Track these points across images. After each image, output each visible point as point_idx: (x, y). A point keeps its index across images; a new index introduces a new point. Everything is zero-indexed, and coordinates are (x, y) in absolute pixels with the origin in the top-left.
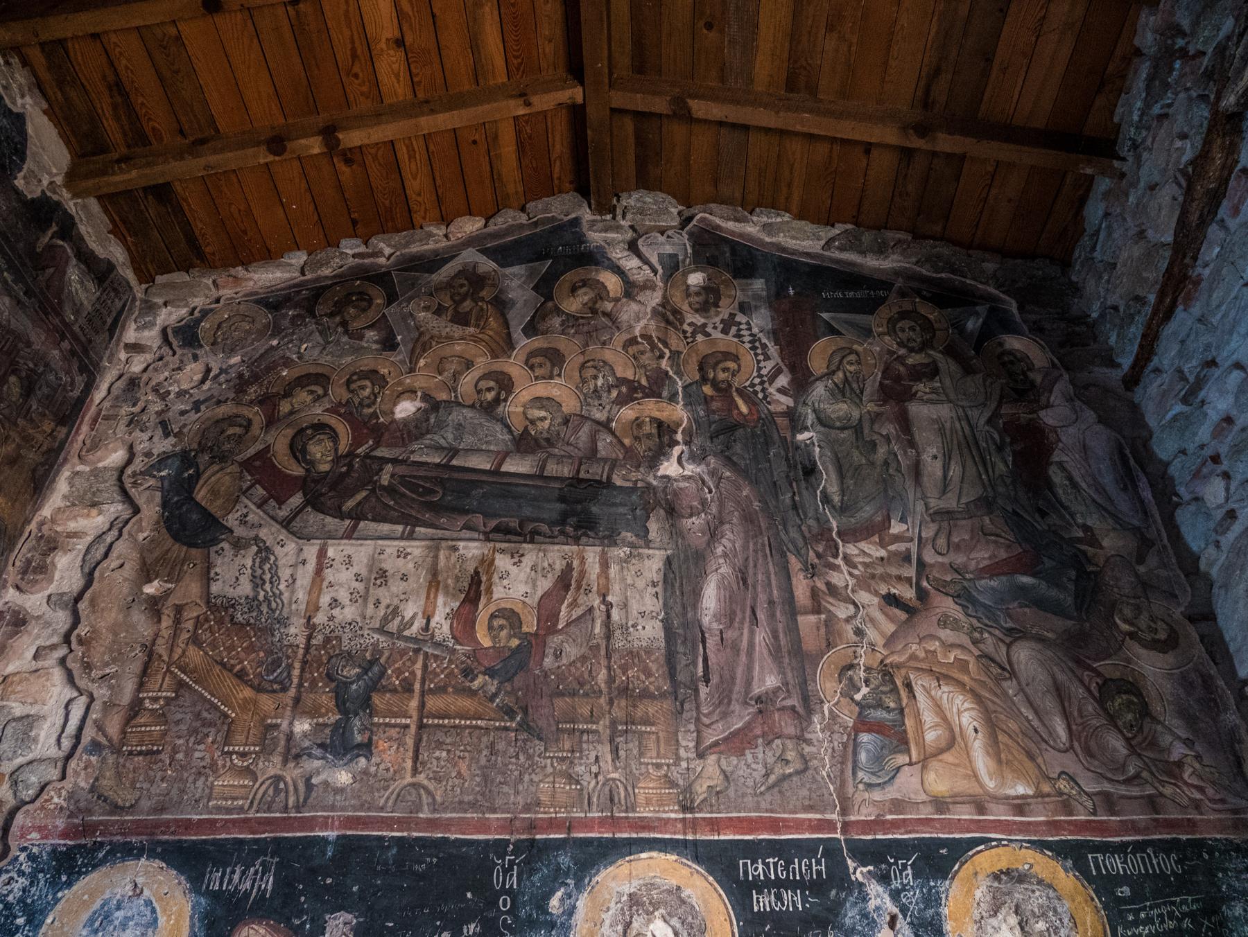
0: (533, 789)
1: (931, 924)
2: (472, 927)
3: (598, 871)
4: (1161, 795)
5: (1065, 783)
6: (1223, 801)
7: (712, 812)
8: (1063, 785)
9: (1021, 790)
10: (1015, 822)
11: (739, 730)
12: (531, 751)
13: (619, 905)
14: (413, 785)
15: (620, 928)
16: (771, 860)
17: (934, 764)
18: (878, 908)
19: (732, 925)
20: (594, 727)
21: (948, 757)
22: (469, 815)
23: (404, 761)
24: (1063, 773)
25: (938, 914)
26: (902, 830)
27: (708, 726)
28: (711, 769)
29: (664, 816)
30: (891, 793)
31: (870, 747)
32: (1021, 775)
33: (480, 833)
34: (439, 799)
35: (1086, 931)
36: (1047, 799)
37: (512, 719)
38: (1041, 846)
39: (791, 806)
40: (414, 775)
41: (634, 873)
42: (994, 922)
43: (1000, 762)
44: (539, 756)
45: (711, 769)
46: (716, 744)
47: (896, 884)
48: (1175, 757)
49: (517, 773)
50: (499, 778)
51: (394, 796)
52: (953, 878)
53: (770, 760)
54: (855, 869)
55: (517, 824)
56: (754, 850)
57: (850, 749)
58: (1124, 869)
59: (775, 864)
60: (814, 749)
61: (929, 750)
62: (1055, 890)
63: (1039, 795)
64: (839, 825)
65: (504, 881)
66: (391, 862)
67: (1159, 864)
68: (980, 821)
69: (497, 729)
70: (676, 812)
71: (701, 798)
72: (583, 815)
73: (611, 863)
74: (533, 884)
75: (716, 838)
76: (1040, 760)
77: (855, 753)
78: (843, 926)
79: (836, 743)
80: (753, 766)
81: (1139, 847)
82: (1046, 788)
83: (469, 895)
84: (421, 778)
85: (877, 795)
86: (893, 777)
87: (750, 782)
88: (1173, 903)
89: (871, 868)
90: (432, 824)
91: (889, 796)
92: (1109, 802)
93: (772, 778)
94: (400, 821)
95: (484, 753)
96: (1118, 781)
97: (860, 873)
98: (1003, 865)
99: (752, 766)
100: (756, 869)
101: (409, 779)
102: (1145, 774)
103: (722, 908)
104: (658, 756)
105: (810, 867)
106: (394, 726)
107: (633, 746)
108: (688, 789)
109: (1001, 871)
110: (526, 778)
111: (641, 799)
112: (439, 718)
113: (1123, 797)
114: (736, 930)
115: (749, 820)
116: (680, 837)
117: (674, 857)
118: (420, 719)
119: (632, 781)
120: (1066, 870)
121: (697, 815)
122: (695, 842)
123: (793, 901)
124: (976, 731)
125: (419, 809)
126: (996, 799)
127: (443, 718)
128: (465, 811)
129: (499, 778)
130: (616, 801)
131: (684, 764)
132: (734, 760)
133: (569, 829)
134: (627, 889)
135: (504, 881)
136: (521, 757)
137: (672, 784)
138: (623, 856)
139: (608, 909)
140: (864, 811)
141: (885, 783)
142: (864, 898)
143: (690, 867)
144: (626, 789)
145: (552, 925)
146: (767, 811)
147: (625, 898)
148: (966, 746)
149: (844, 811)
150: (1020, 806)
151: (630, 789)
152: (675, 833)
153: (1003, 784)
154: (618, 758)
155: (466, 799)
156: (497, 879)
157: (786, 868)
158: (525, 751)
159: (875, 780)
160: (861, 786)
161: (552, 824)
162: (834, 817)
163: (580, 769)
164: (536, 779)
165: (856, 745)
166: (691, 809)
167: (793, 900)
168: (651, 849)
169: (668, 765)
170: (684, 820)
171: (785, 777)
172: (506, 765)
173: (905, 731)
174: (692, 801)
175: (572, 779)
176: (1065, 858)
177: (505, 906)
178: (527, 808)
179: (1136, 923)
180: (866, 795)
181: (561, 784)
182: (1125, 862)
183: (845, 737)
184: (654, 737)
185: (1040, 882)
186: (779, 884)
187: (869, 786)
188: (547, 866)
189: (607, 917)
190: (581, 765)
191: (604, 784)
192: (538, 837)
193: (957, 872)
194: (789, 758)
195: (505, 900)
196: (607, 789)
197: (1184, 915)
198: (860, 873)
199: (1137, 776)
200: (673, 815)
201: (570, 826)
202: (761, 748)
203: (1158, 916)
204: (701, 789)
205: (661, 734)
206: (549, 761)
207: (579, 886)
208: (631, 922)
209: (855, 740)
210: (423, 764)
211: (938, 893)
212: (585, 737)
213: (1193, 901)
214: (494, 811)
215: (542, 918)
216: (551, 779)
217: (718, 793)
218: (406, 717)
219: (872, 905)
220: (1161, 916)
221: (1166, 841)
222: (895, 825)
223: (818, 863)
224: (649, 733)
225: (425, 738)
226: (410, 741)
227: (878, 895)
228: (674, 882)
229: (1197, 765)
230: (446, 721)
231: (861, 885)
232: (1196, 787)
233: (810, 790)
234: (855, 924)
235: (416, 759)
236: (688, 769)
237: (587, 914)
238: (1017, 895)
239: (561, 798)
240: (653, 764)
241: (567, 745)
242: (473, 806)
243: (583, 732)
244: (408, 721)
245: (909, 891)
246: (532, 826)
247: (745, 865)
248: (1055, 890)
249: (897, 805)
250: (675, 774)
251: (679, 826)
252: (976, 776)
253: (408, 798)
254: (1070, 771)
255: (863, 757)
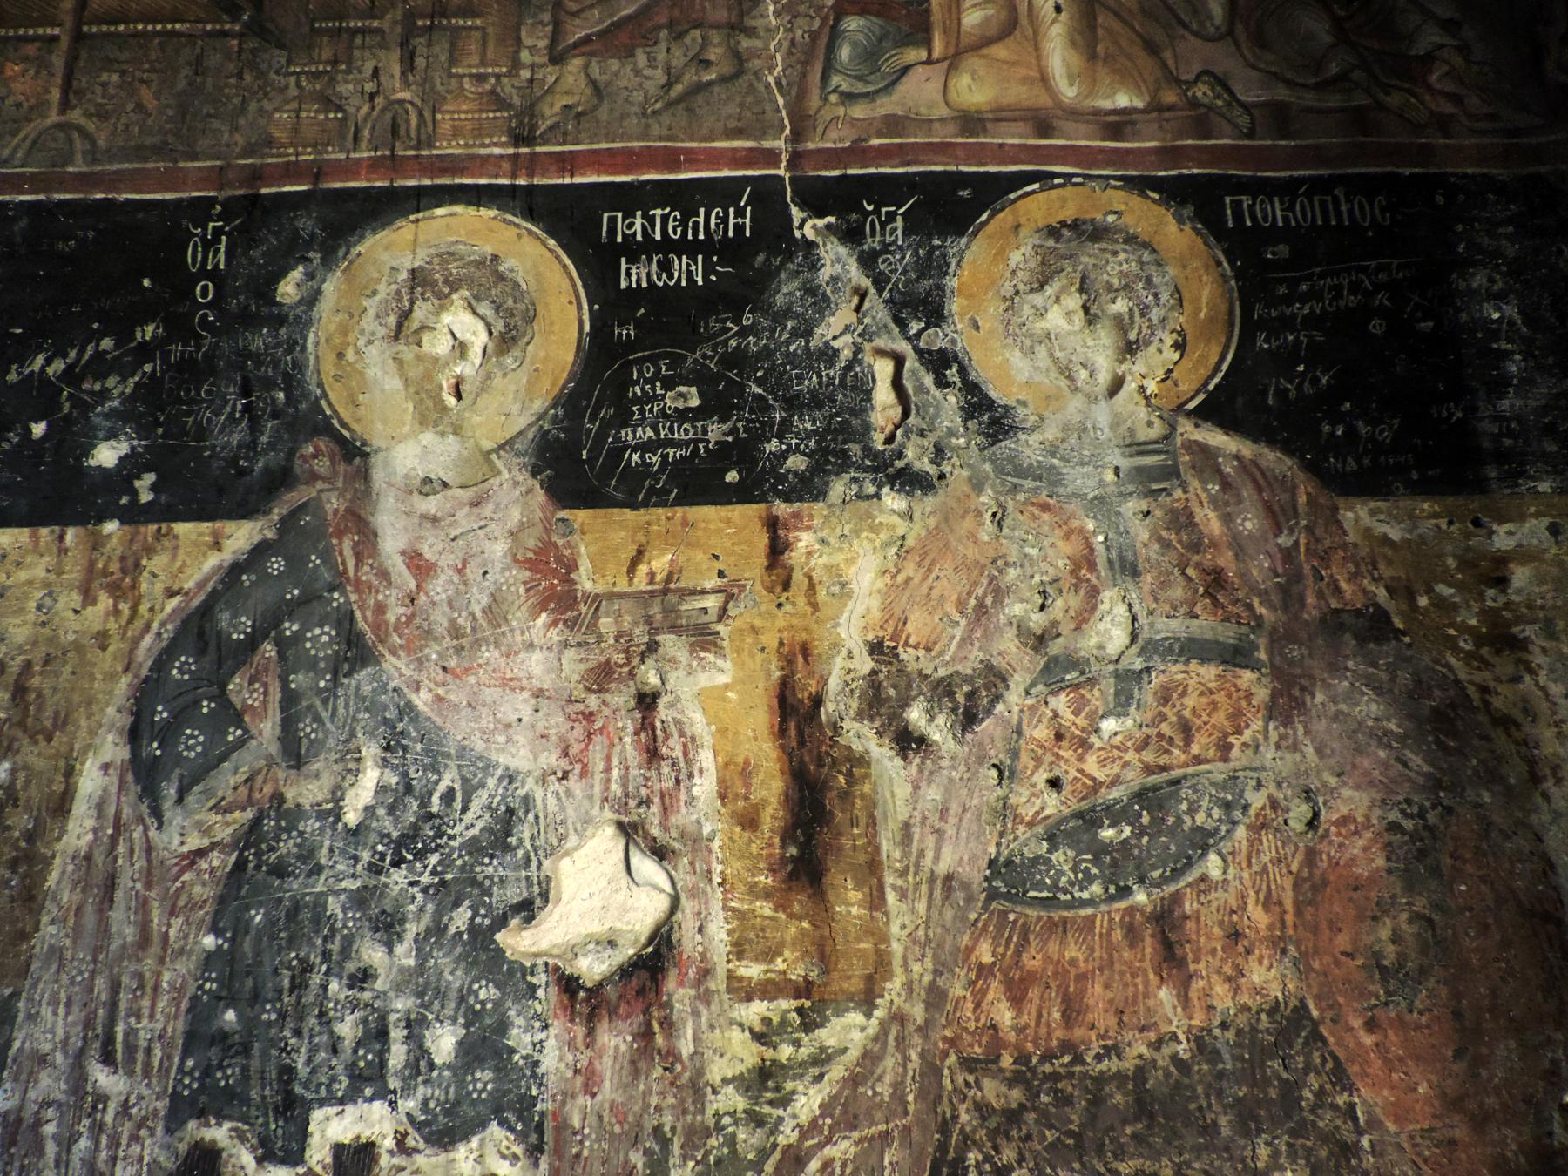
0: (262, 122)
1: (924, 302)
2: (150, 329)
3: (362, 237)
4: (1381, 107)
5: (1205, 88)
6: (1492, 117)
7: (564, 143)
8: (1201, 91)
9: (1123, 100)
10: (1102, 150)
11: (629, 18)
12: (264, 66)
13: (394, 287)
14: (59, 126)
15: (392, 320)
16: (659, 212)
17: (973, 62)
18: (834, 279)
19: (580, 307)
20: (375, 24)
21: (1000, 51)
22: (151, 165)
23: (47, 91)
24: (1206, 72)
25: (940, 288)
26: (897, 161)
27: (575, 14)
28: (571, 79)
29: (483, 151)
30: (887, 106)
31: (861, 37)
32: (1125, 77)
33: (167, 190)
34: (101, 143)
35: (1198, 310)
36: (1167, 115)
37: (235, 19)
38: (1139, 185)
39: (704, 132)
40: (62, 111)
41: (421, 238)
42: (1038, 299)
43: (1092, 57)
44: (277, 72)
45: (571, 79)
46: (587, 40)
47: (872, 243)
48: (1420, 48)
49: (237, 101)
50: (208, 109)
51: (28, 143)
52: (975, 234)
53: (678, 60)
54: (803, 221)
55: (231, 175)
56: (630, 198)
57: (824, 39)
58: (1285, 218)
59: (665, 218)
60: (758, 43)
61: (965, 41)
62: (1154, 251)
63: (1155, 107)
64: (785, 157)
65: (205, 259)
66: (19, 240)
67: (1351, 212)
68: (1039, 147)
69: (209, 34)
70: (502, 145)
71: (549, 122)
72: (343, 156)
73: (383, 226)
74: (252, 262)
75: (567, 181)
76: (1167, 55)
77: (831, 47)
78: (770, 306)
79: (799, 33)
80: (646, 72)
81: (1318, 186)
82: (1170, 97)
83: (146, 283)
84: (76, 116)
85: (859, 111)
86: (894, 83)
87: (638, 97)
88: (1364, 270)
89: (831, 219)
90: (85, 181)
91: (883, 111)
92: (1279, 118)
93: (678, 89)
94: (32, 178)
95: (185, 71)
96: (1303, 86)
97: (810, 228)
98: (1068, 214)
99: (641, 75)
100: (631, 225)
101: (54, 118)
102: (1357, 75)
103: (566, 284)
104: (483, 63)
105: (725, 220)
106: (36, 38)
107: (441, 52)
108: (530, 111)
109: (1063, 224)
110: (253, 106)
111: (445, 127)
112: (109, 23)
113: (1309, 110)
114: (586, 318)
115: (629, 152)
116: (506, 181)
117: (493, 213)
118: (79, 23)
119: (432, 102)
120: (1180, 221)
121: (538, 149)
122: (530, 189)
123: (689, 273)
124: (1058, 9)
125: (68, 159)
126: (1074, 114)
127: (116, 23)
128: (146, 160)
129: (208, 109)
130: (402, 132)
131: (525, 74)
132: (614, 64)
133: (317, 178)
134: (407, 262)
135: (205, 259)
136: (248, 78)
137: (499, 102)
138: (405, 215)
139: (375, 293)
140: (833, 134)
141: (877, 92)
142: (814, 265)
143: (517, 226)
144: (421, 115)
145: (281, 320)
146: (661, 139)
147: (404, 275)
148: (1036, 33)
149: (797, 136)
150: (1118, 124)
151: (427, 114)
152: (496, 177)
153: (1091, 93)
154: (412, 68)
155: (149, 141)
156: (192, 255)
157: (683, 223)
158: (253, 66)
159: (861, 88)
160: (833, 98)
161: (291, 171)
162: (780, 144)
163: (345, 89)
164: (266, 105)
165: (835, 35)
166: (529, 141)
167: (688, 270)
168: (453, 202)
169: (498, 76)
170: (516, 156)
171: (700, 88)
172: (221, 89)
173: (928, 12)
174: (533, 128)
175: (329, 102)
176: (1182, 203)
177: (204, 295)
178: (249, 151)
179: (1288, 300)
180: (841, 111)
181: (310, 112)
182: (1291, 208)
183: (817, 23)
184: (477, 34)
185: (1131, 239)
186: (668, 247)
187: (849, 98)
188: (276, 234)
189: (372, 305)
190: (346, 82)
191: (383, 111)
192: (264, 191)
193: (984, 224)
194: (712, 58)
195: (205, 288)
196: (388, 116)
197: (1378, 287)
198: (810, 228)
199: (1343, 77)
200: (497, 151)
201: (318, 172)
202: (663, 46)
203: (1331, 288)
204: (551, 111)
205: (490, 30)
206: (292, 79)
207: (329, 262)
208: (411, 310)
209: (834, 27)
210: (80, 93)
211: (944, 256)
212: (358, 40)
213: (1400, 267)
214: (194, 157)
215: (265, 310)
216: (295, 105)
217: (579, 115)
218: (53, 25)
219: (825, 274)
220: (1338, 289)
221: (1374, 176)
222: (884, 154)
223: (740, 213)
224: (470, 28)
225: (84, 54)
226: (58, 62)
227: (838, 260)
228: (489, 250)
229: (1458, 61)
230: (121, 28)
231: (811, 245)
232: (1450, 96)
233: (742, 105)
234: (792, 303)
235: (67, 88)
236: (531, 81)
237: (338, 302)
238: (1085, 259)
239: (309, 133)
240: (471, 76)
241: (327, 54)
242: (159, 151)
243: (357, 31)
244: (57, 31)
245: (893, 253)
246: (256, 176)
247: (613, 220)
248: (1154, 251)
249: (893, 124)
250: (508, 88)
251: (506, 166)
252: (1044, 79)
253: (53, 145)
254: (1217, 70)
255: (845, 53)
